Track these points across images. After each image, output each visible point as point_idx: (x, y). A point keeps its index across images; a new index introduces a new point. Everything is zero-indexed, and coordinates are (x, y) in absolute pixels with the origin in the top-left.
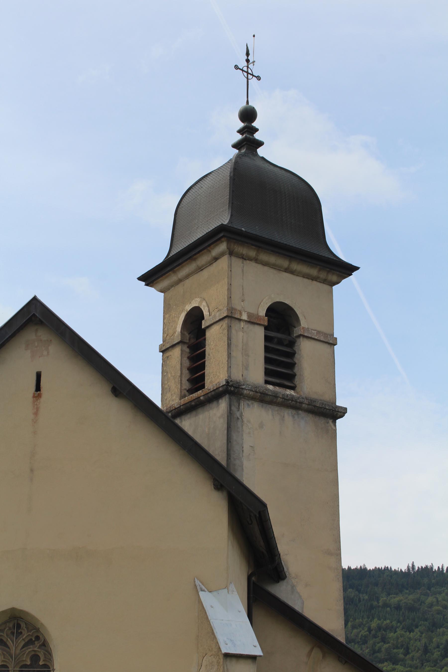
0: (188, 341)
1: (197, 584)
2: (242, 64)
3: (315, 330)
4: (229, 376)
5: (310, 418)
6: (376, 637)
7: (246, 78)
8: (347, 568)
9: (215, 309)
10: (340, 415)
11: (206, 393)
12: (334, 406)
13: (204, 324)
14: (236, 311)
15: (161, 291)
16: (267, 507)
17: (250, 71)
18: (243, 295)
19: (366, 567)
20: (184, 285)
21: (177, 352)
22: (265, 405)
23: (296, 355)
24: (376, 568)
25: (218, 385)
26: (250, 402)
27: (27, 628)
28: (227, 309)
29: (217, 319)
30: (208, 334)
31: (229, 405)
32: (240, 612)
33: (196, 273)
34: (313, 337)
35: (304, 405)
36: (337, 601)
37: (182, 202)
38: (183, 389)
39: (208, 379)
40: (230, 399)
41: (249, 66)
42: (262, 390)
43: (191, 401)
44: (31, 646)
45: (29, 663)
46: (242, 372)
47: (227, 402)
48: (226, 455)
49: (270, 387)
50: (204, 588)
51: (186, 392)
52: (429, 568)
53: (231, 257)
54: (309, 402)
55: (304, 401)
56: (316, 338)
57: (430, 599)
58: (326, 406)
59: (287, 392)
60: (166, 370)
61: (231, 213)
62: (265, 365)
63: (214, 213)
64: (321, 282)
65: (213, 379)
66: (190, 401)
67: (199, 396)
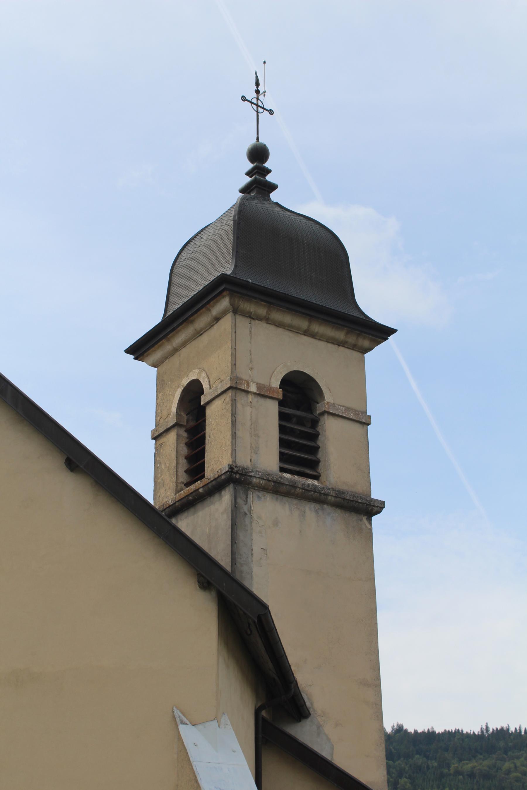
0: (185, 424)
2: (251, 95)
5: (338, 514)
7: (255, 111)
8: (413, 732)
9: (216, 381)
10: (376, 510)
11: (206, 483)
12: (368, 499)
13: (204, 400)
14: (243, 382)
15: (154, 366)
16: (269, 609)
17: (260, 104)
18: (251, 362)
19: (434, 730)
20: (180, 356)
21: (172, 437)
22: (280, 498)
23: (320, 436)
24: (445, 730)
25: (219, 472)
26: (261, 494)
28: (231, 378)
29: (219, 392)
30: (210, 412)
31: (233, 496)
32: (234, 752)
33: (193, 339)
34: (341, 415)
35: (330, 498)
36: (377, 745)
37: (179, 258)
38: (179, 483)
39: (209, 467)
40: (235, 489)
41: (259, 97)
42: (276, 478)
43: (188, 496)
46: (251, 456)
47: (231, 494)
48: (231, 559)
49: (288, 476)
50: (185, 720)
51: (183, 485)
52: (505, 730)
53: (235, 315)
54: (336, 494)
55: (330, 493)
56: (345, 415)
57: (507, 765)
58: (358, 499)
59: (309, 482)
60: (159, 460)
61: (236, 263)
62: (279, 448)
63: (215, 266)
65: (215, 466)
66: (186, 495)
67: (198, 488)
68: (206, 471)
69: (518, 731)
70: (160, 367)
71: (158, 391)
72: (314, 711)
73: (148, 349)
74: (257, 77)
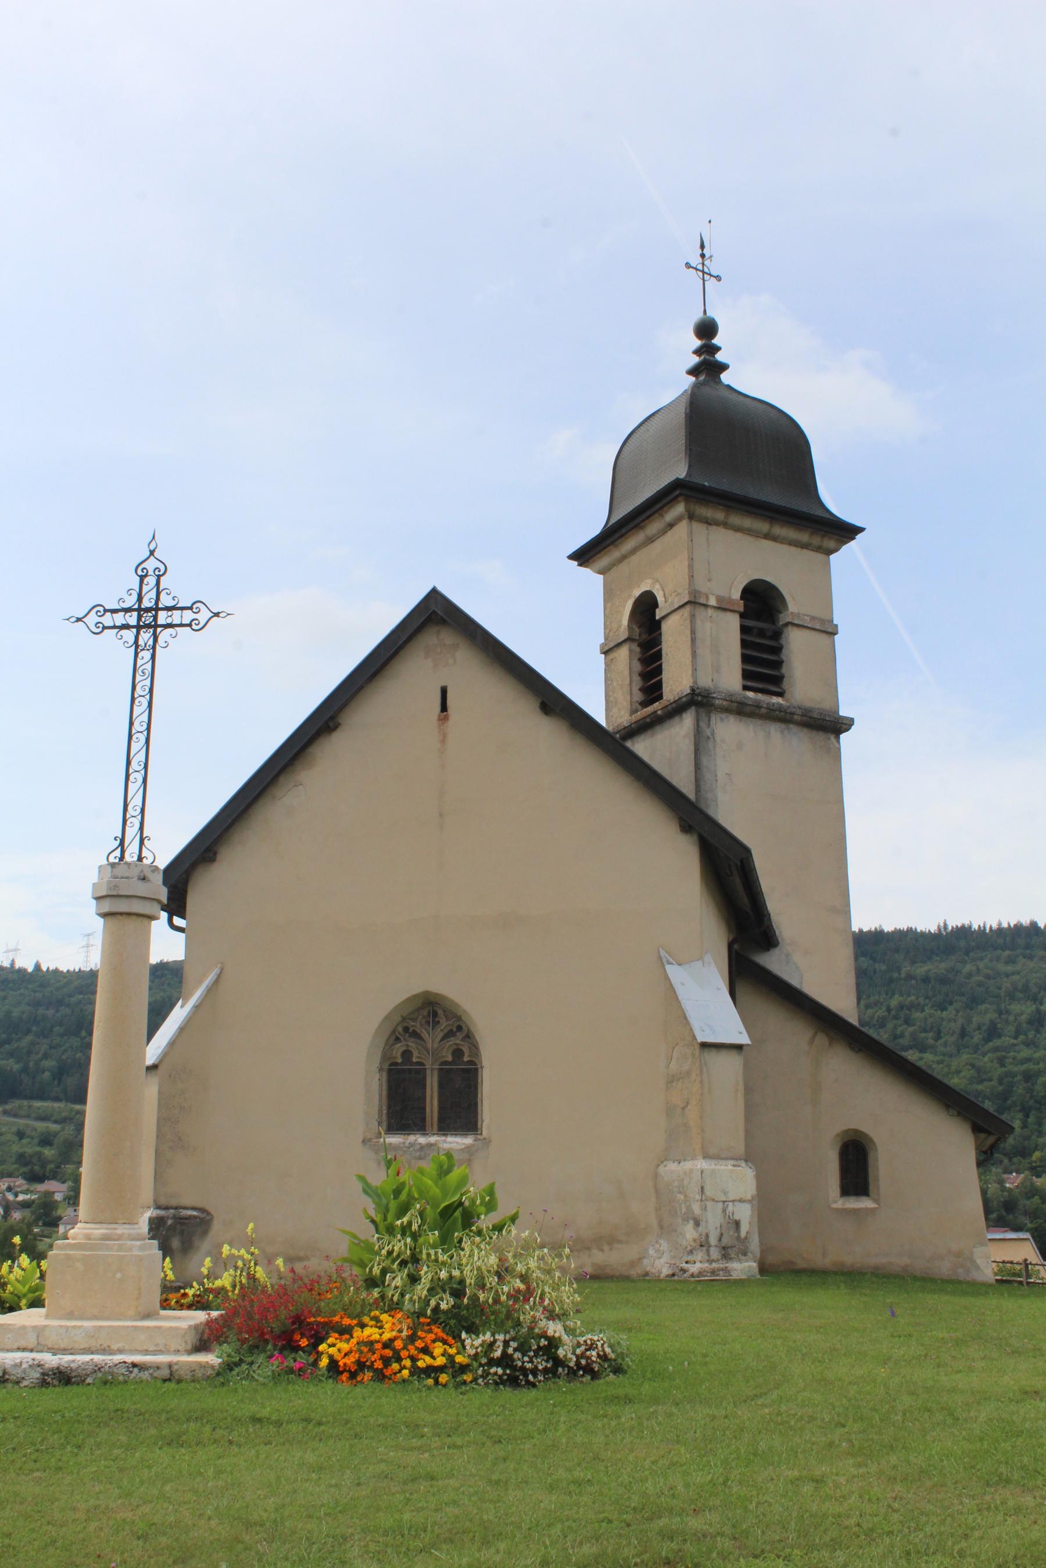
0: (637, 638)
2: (696, 261)
3: (808, 616)
4: (695, 682)
6: (897, 1019)
8: (857, 931)
15: (600, 572)
17: (706, 270)
18: (709, 572)
22: (744, 718)
24: (896, 929)
26: (724, 716)
27: (446, 1017)
30: (665, 627)
35: (796, 717)
40: (697, 712)
43: (645, 718)
44: (452, 1039)
45: (450, 1059)
49: (750, 694)
50: (671, 960)
51: (638, 705)
57: (968, 968)
61: (690, 462)
64: (814, 551)
68: (664, 688)
69: (982, 929)
71: (606, 601)
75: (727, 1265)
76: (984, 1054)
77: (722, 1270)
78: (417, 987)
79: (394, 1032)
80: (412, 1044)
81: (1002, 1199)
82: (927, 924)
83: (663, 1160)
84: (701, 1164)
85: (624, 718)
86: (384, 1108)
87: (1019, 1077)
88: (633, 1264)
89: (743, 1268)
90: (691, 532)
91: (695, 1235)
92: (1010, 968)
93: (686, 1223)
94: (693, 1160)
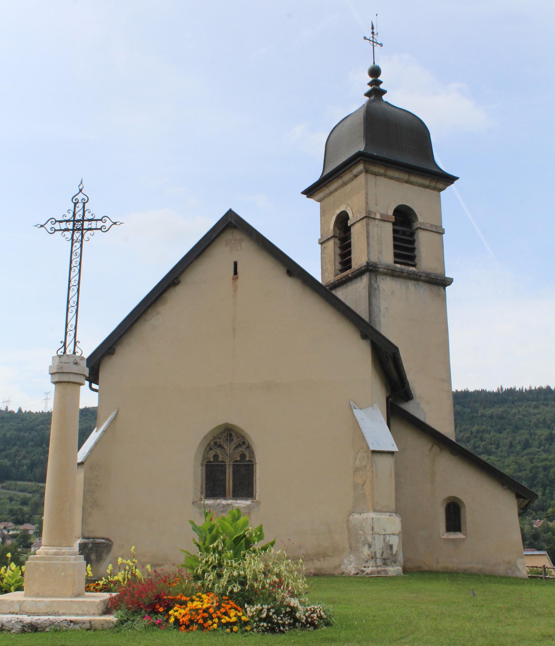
0: (338, 236)
1: (351, 404)
2: (369, 36)
3: (429, 224)
4: (369, 259)
8: (455, 391)
15: (318, 201)
17: (375, 40)
18: (376, 201)
22: (395, 278)
23: (416, 242)
24: (475, 390)
26: (384, 277)
27: (237, 436)
28: (366, 211)
29: (359, 219)
30: (353, 230)
35: (422, 278)
43: (342, 278)
44: (240, 448)
45: (239, 459)
49: (398, 266)
50: (356, 407)
51: (338, 271)
57: (514, 411)
61: (366, 142)
70: (322, 202)
72: (415, 396)
73: (315, 192)
74: (372, 24)
75: (386, 568)
76: (522, 457)
77: (383, 571)
78: (221, 421)
79: (209, 445)
80: (219, 451)
81: (532, 534)
82: (492, 387)
83: (351, 513)
84: (372, 515)
85: (331, 278)
86: (204, 485)
87: (541, 469)
88: (336, 568)
89: (394, 570)
90: (367, 180)
91: (369, 552)
92: (536, 411)
93: (364, 546)
94: (367, 512)
